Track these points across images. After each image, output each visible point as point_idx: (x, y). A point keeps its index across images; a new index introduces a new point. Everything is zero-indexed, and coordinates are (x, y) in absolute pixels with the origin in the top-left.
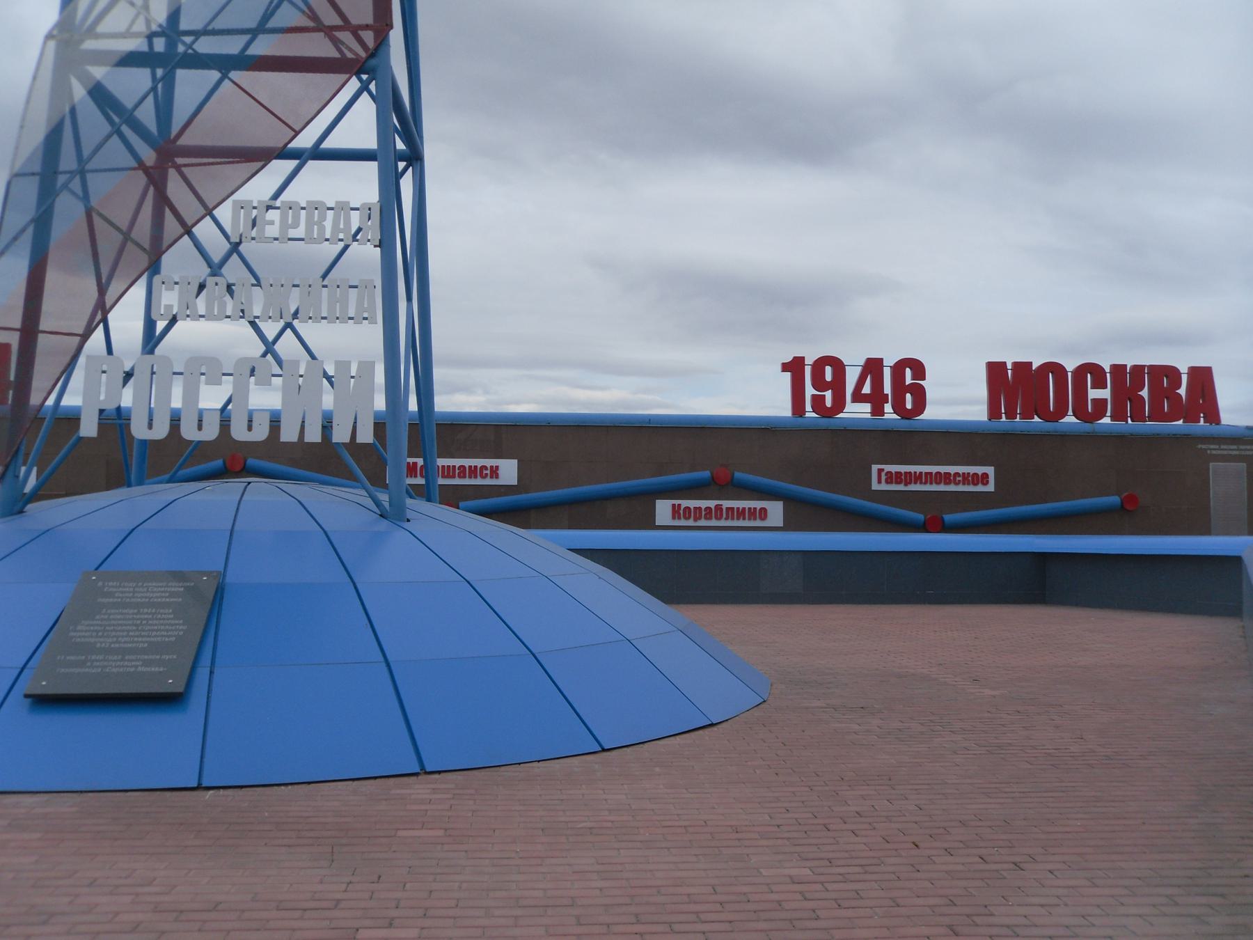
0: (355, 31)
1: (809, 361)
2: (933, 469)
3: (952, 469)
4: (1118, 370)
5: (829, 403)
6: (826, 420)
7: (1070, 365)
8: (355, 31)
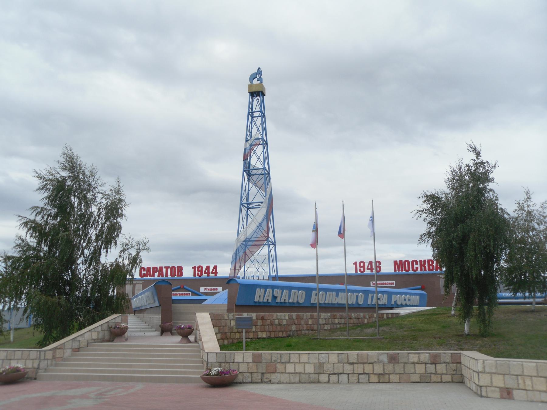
0: (265, 237)
2: (383, 282)
3: (386, 282)
4: (421, 261)
5: (362, 270)
7: (410, 261)
8: (265, 237)
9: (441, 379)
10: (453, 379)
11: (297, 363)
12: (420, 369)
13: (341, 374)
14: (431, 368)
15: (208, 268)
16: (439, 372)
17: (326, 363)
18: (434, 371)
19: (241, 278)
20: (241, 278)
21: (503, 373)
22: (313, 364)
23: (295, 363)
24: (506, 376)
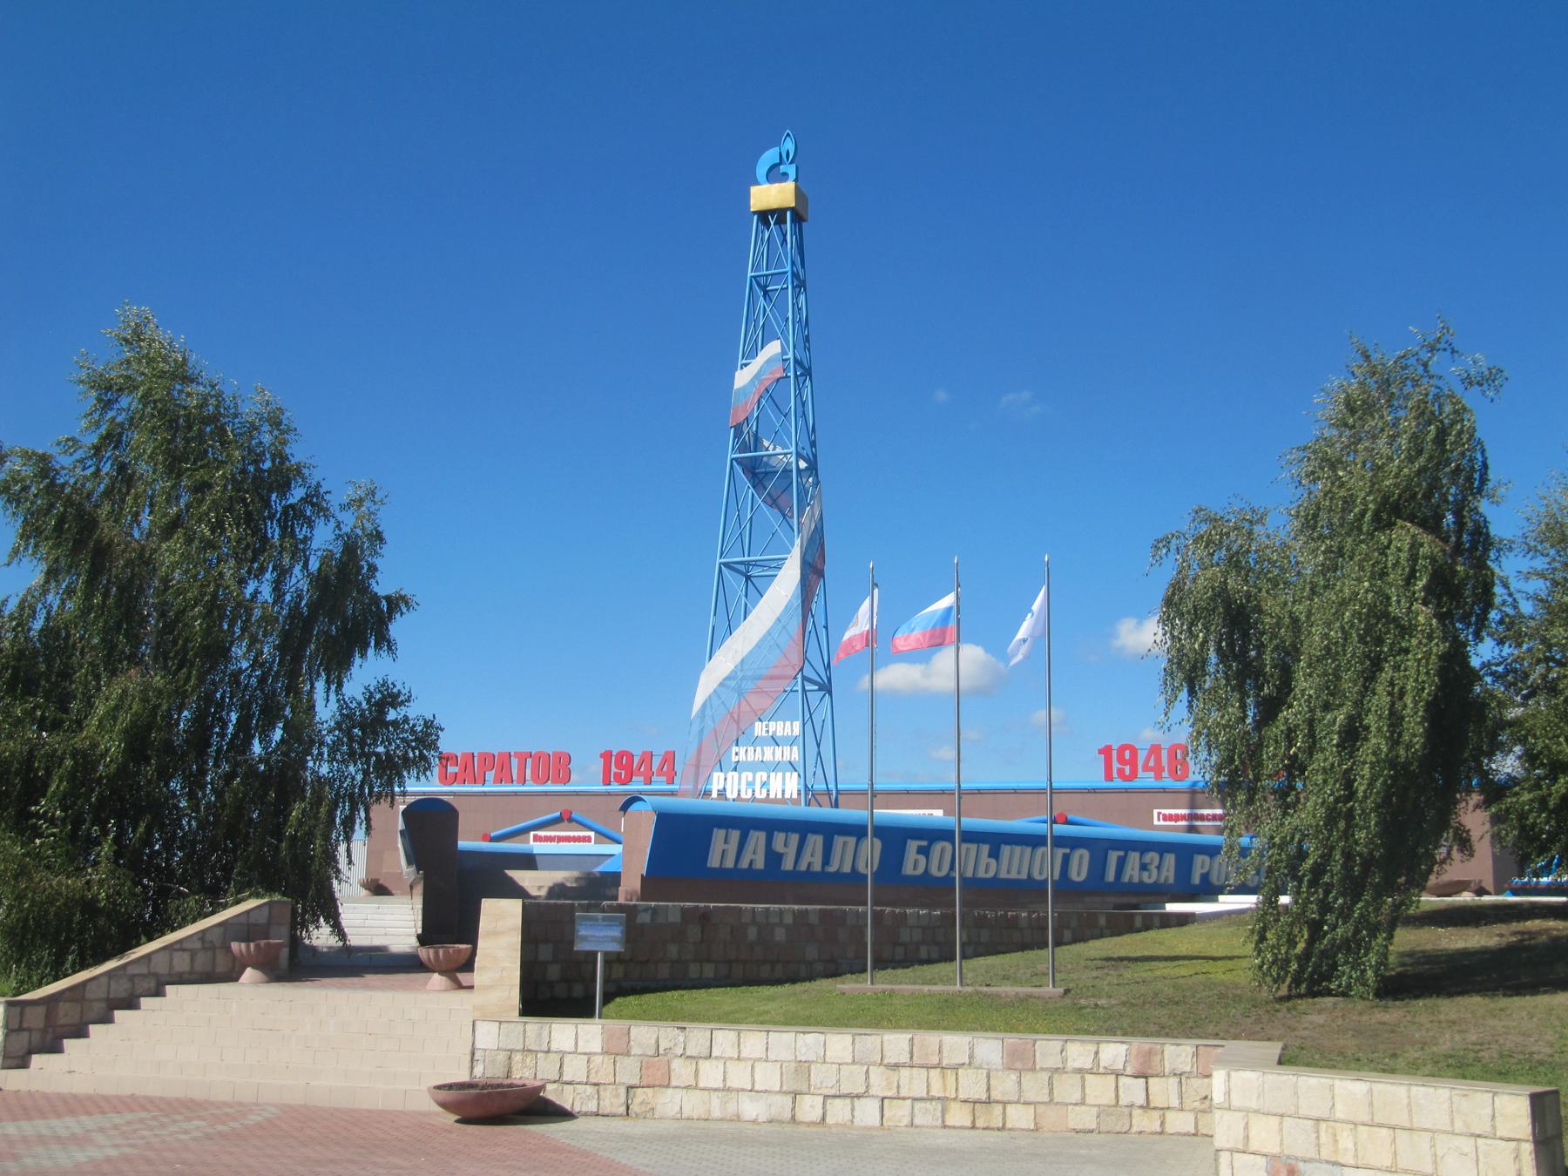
1: (1115, 747)
5: (1127, 772)
6: (1179, 783)
9: (1162, 1124)
10: (1200, 1127)
11: (731, 1058)
12: (1102, 1092)
13: (858, 1096)
14: (1133, 1090)
15: (669, 758)
16: (1156, 1101)
17: (817, 1062)
18: (1141, 1100)
19: (714, 795)
20: (714, 795)
21: (1280, 1111)
22: (779, 1065)
23: (726, 1060)
24: (1288, 1121)
